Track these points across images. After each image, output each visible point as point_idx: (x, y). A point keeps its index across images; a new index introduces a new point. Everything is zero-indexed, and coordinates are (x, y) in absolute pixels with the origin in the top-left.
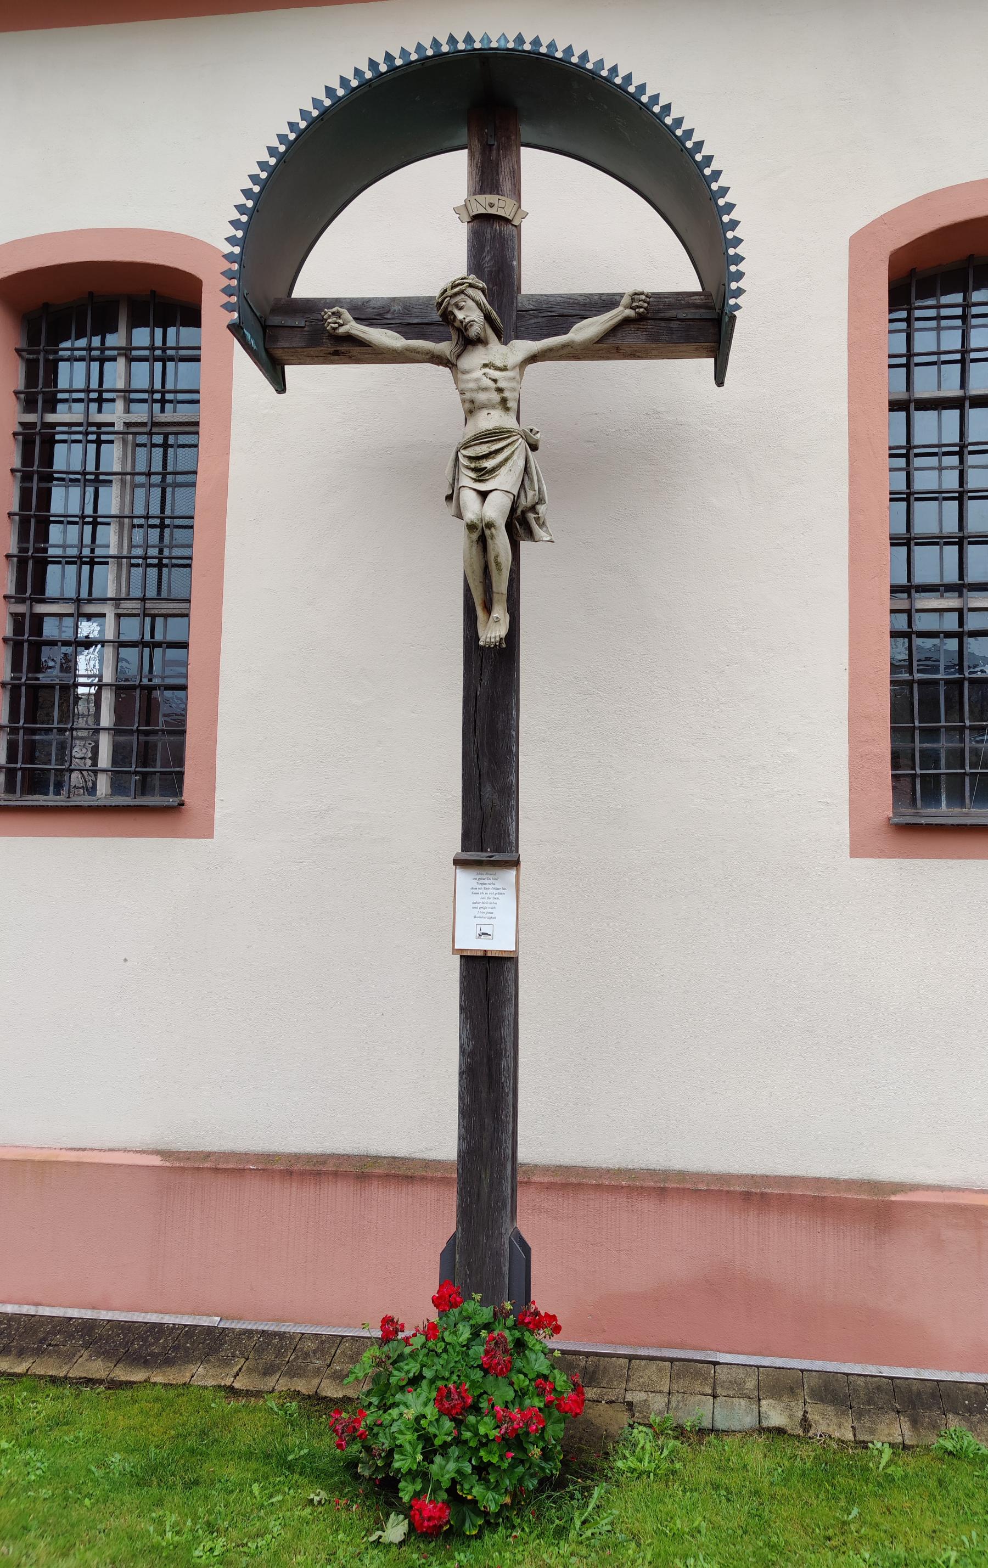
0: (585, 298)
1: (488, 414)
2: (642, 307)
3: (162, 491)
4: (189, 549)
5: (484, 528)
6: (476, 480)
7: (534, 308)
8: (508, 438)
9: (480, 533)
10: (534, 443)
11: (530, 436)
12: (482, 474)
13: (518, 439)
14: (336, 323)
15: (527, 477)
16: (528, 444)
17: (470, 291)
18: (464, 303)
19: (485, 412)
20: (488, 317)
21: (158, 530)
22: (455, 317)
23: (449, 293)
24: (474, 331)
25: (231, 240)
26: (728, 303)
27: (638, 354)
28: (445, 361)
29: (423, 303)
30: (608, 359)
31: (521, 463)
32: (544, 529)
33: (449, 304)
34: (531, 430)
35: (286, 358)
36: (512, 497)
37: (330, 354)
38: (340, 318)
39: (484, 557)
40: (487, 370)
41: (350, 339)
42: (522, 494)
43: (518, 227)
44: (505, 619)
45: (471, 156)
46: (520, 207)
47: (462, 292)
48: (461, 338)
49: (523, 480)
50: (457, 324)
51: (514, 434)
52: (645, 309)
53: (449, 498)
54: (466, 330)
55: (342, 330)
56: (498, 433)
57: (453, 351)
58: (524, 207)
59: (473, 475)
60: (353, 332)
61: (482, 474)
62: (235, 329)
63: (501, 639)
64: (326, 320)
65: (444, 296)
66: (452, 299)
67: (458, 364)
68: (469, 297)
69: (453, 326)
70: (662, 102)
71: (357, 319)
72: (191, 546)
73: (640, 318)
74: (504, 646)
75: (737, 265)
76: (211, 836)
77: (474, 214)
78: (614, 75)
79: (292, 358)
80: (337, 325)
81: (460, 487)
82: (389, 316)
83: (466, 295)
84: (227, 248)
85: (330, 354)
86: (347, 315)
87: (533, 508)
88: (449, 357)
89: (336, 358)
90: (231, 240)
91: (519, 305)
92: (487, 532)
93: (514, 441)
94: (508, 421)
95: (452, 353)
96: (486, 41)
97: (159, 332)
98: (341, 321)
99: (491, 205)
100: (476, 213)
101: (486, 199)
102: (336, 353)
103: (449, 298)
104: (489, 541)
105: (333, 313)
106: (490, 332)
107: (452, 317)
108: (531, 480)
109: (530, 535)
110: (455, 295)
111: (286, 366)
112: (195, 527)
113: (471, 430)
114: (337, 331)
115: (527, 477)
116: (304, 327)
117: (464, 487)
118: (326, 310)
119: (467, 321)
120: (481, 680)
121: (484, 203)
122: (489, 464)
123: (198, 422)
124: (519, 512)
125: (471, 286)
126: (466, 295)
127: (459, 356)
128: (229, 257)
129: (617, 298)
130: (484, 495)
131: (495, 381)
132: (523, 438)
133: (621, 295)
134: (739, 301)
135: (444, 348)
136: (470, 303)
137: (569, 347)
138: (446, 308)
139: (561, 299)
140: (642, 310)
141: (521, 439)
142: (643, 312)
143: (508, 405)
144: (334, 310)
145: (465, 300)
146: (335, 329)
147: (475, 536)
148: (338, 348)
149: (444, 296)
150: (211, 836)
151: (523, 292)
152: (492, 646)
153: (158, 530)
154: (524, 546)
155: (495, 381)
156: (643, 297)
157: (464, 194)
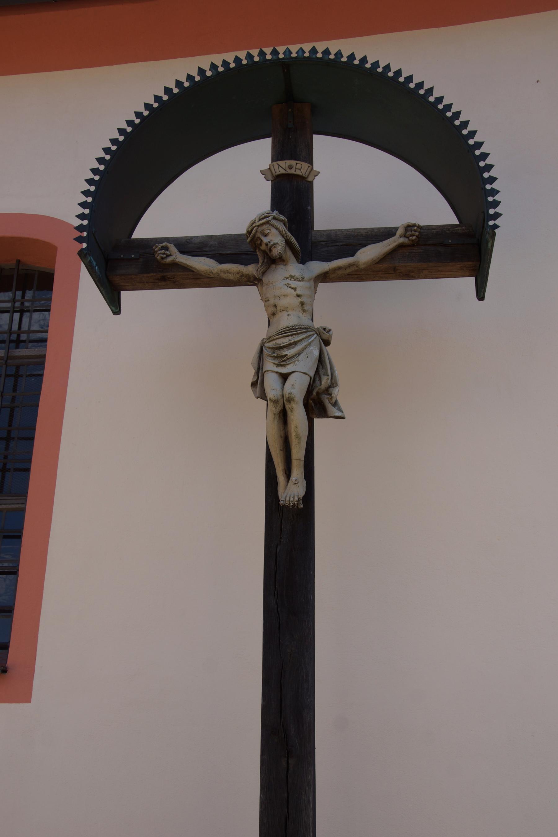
0: (366, 231)
1: (288, 315)
2: (414, 236)
3: (11, 411)
4: (24, 505)
5: (285, 403)
6: (278, 365)
7: (326, 240)
8: (306, 332)
9: (282, 407)
10: (327, 339)
11: (324, 333)
12: (282, 360)
13: (313, 335)
14: (164, 254)
15: (321, 366)
16: (322, 339)
17: (274, 222)
18: (269, 231)
19: (285, 313)
20: (288, 243)
21: (13, 378)
22: (262, 241)
23: (258, 223)
24: (276, 252)
25: (81, 217)
26: (488, 224)
27: (412, 274)
28: (252, 279)
29: (235, 239)
30: (386, 279)
31: (316, 353)
32: (337, 408)
33: (256, 232)
34: (324, 329)
35: (122, 284)
36: (309, 379)
37: (158, 279)
38: (168, 251)
39: (285, 428)
40: (288, 281)
41: (175, 265)
42: (317, 379)
43: (311, 183)
44: (302, 485)
45: (273, 142)
46: (313, 168)
47: (268, 222)
48: (266, 260)
49: (317, 368)
50: (263, 247)
51: (310, 330)
52: (417, 236)
53: (254, 384)
54: (270, 250)
55: (169, 260)
56: (297, 329)
57: (260, 269)
58: (315, 168)
59: (276, 362)
60: (178, 260)
61: (282, 360)
62: (82, 254)
63: (299, 500)
64: (157, 252)
65: (254, 225)
66: (260, 228)
67: (263, 279)
68: (273, 226)
69: (260, 249)
70: (426, 87)
71: (182, 252)
72: (47, 332)
73: (413, 245)
74: (302, 506)
75: (493, 197)
76: (28, 701)
77: (277, 174)
78: (387, 70)
79: (127, 284)
80: (165, 255)
81: (265, 372)
82: (207, 249)
83: (271, 225)
84: (77, 222)
85: (158, 279)
86: (173, 249)
87: (328, 391)
88: (256, 275)
89: (163, 283)
90: (81, 217)
91: (313, 238)
92: (287, 406)
93: (310, 336)
94: (305, 321)
95: (259, 270)
96: (287, 53)
97: (19, 294)
98: (168, 252)
99: (291, 167)
100: (278, 173)
101: (284, 164)
102: (163, 279)
103: (256, 227)
104: (289, 413)
105: (162, 247)
106: (289, 253)
107: (259, 242)
108: (324, 367)
109: (324, 414)
110: (262, 225)
111: (122, 292)
112: (20, 572)
113: (274, 329)
114: (165, 260)
115: (321, 366)
116: (139, 259)
117: (268, 371)
118: (157, 244)
119: (271, 244)
120: (281, 538)
121: (284, 166)
122: (290, 352)
123: (50, 309)
124: (314, 393)
125: (274, 218)
126: (271, 225)
127: (264, 273)
128: (80, 228)
129: (394, 230)
130: (285, 377)
131: (295, 289)
132: (317, 334)
133: (396, 229)
134: (497, 222)
135: (251, 269)
136: (274, 231)
137: (355, 266)
138: (254, 236)
139: (347, 232)
140: (414, 238)
141: (316, 335)
142: (415, 239)
143: (305, 308)
144: (164, 244)
145: (270, 228)
146: (162, 258)
147: (279, 408)
148: (165, 274)
149: (254, 225)
150: (28, 701)
151: (315, 229)
152: (292, 504)
153: (13, 378)
154: (318, 422)
155: (295, 289)
156: (415, 228)
157: (270, 162)
